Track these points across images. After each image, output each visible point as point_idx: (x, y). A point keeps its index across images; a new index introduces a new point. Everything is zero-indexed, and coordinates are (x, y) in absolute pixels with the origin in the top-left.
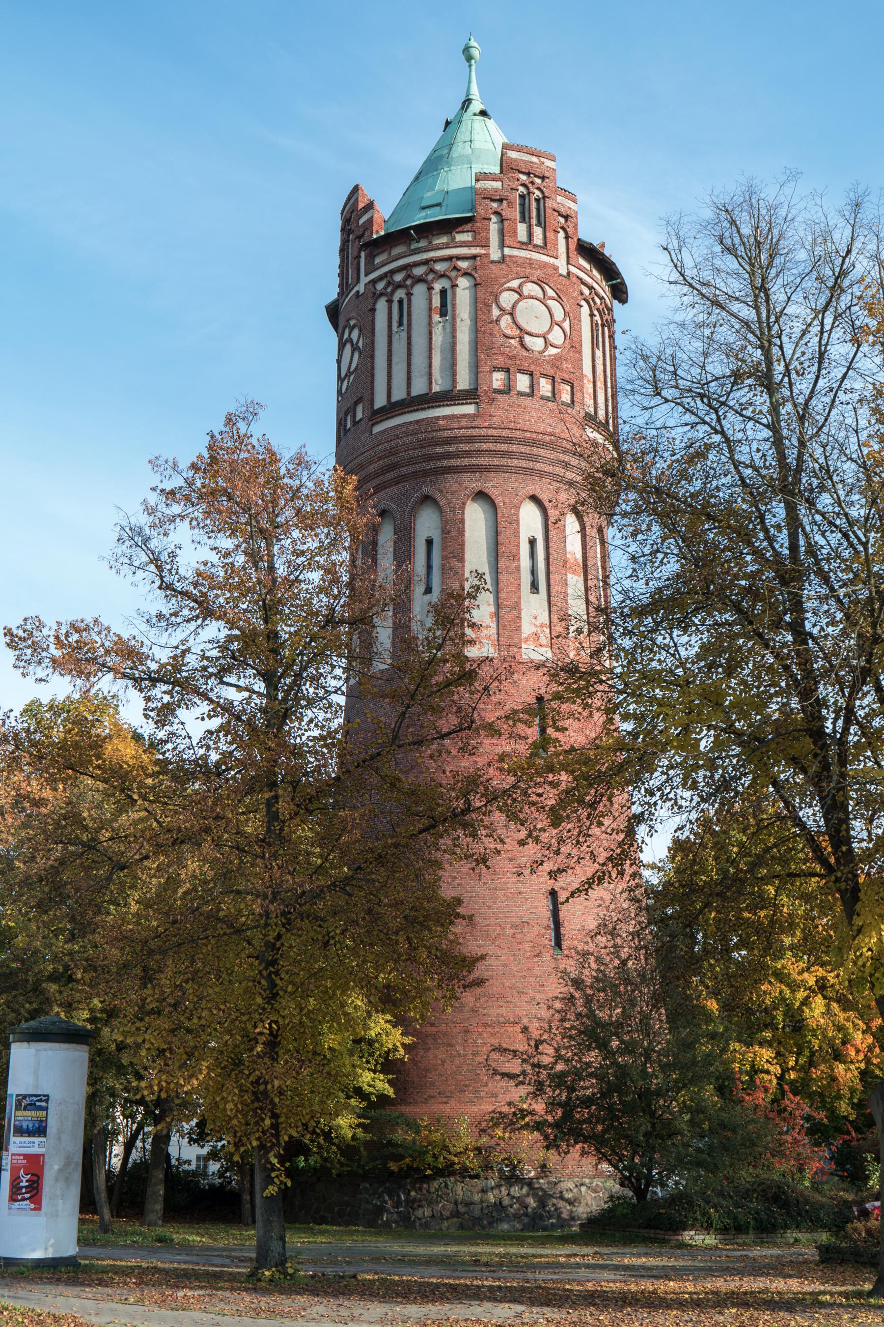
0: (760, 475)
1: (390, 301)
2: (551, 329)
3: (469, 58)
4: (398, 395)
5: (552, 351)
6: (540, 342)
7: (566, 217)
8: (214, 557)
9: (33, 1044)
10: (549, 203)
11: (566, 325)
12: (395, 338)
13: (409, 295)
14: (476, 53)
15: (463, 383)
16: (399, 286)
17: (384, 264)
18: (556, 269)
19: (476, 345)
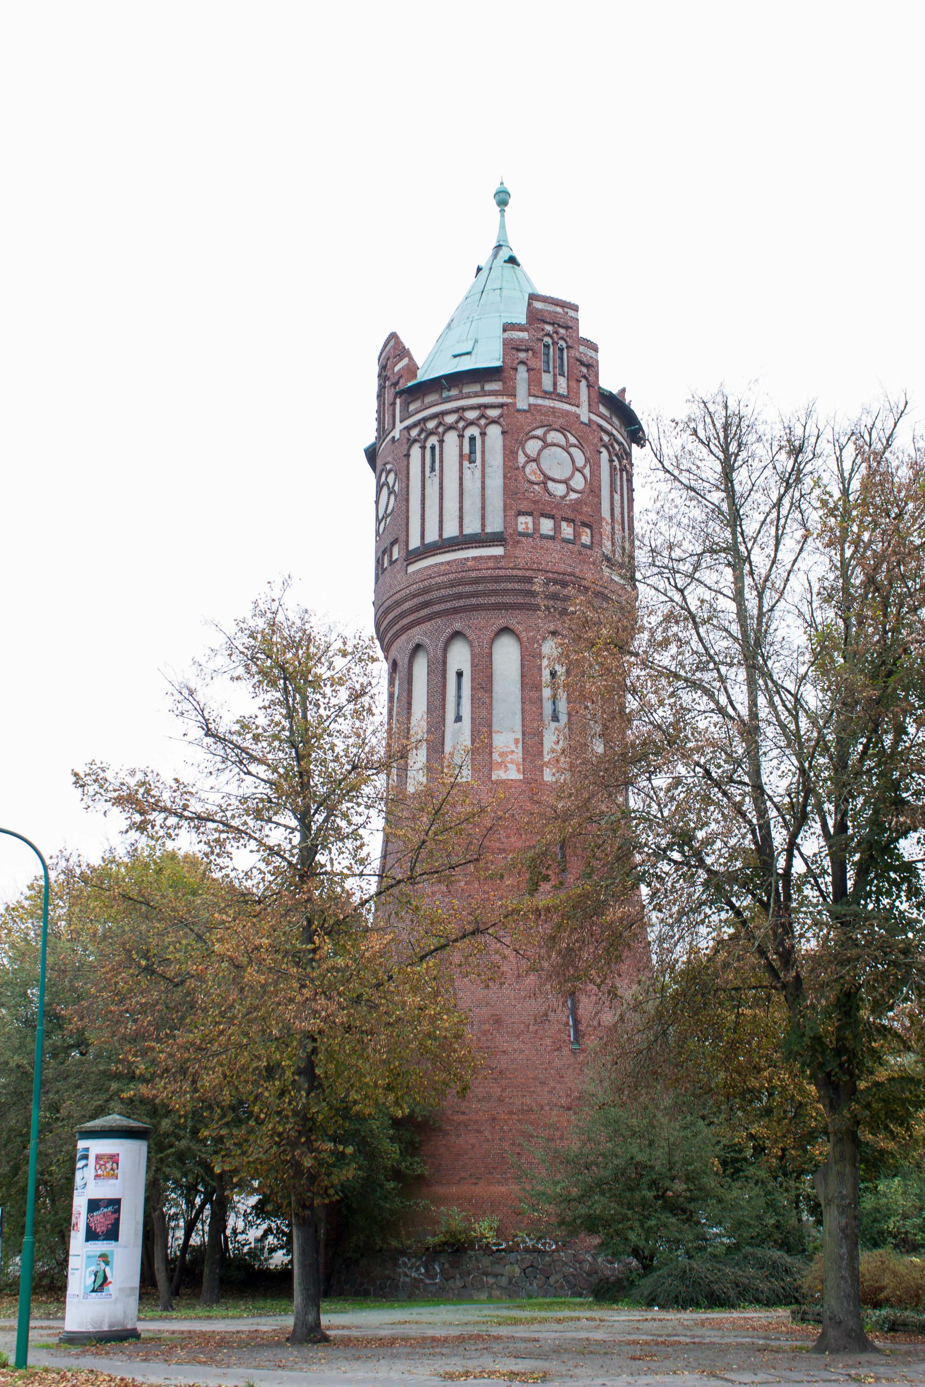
1: (423, 448)
12: (467, 474)
13: (441, 442)
15: (495, 525)
16: (431, 433)
17: (476, 395)
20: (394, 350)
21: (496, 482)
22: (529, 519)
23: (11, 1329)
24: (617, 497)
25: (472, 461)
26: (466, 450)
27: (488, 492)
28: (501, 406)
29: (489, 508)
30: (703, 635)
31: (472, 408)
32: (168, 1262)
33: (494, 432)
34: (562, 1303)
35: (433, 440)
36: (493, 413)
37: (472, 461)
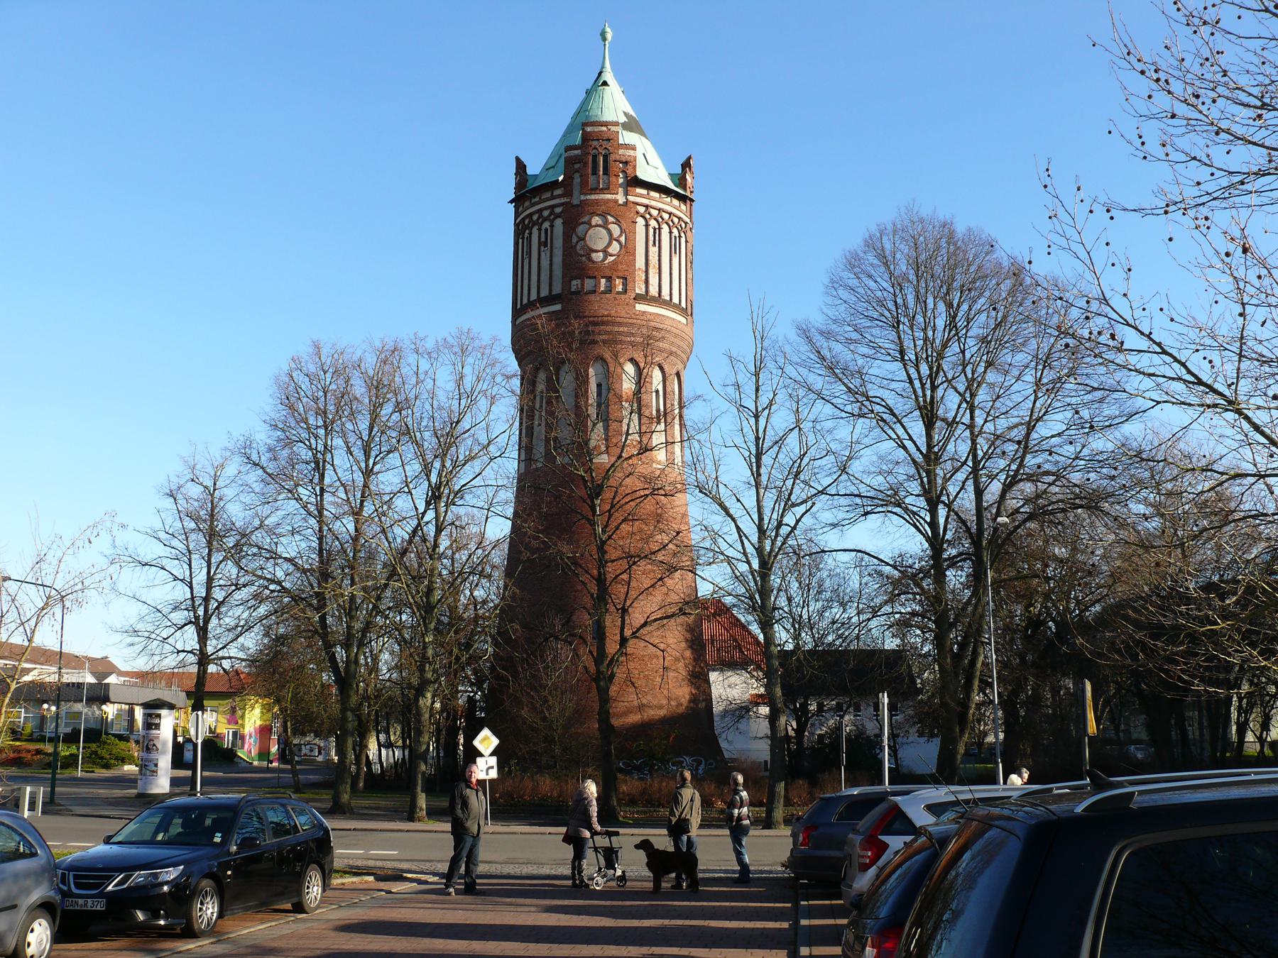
0: (1228, 131)
1: (540, 230)
2: (609, 244)
3: (604, 39)
4: (544, 293)
5: (612, 259)
6: (601, 254)
7: (626, 163)
8: (1251, 57)
9: (774, 951)
10: (612, 157)
11: (623, 239)
12: (543, 254)
13: (552, 226)
14: (609, 36)
15: (557, 289)
16: (545, 219)
17: (548, 199)
18: (616, 201)
19: (565, 264)
20: (521, 166)
21: (558, 259)
22: (579, 281)
23: (704, 871)
24: (653, 251)
25: (546, 245)
26: (543, 239)
27: (554, 267)
28: (562, 204)
29: (554, 278)
30: (52, 576)
31: (546, 208)
32: (1090, 738)
33: (559, 222)
34: (301, 938)
35: (546, 225)
36: (558, 210)
37: (546, 245)
